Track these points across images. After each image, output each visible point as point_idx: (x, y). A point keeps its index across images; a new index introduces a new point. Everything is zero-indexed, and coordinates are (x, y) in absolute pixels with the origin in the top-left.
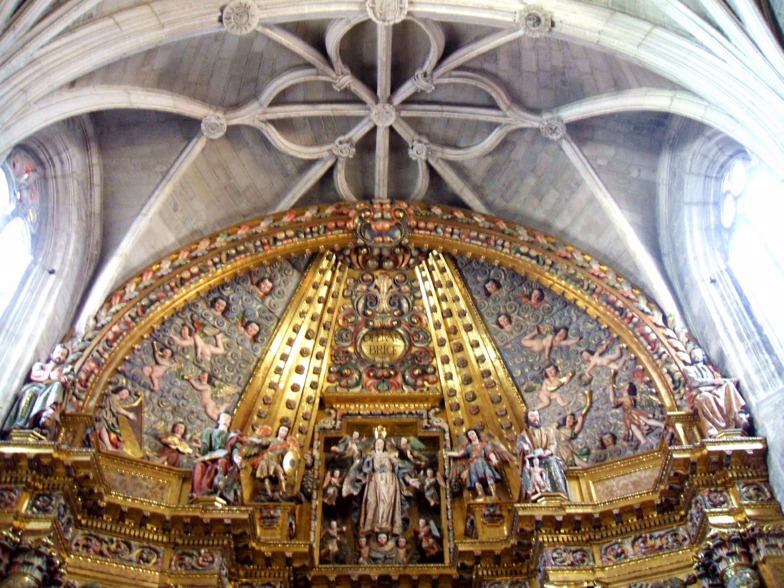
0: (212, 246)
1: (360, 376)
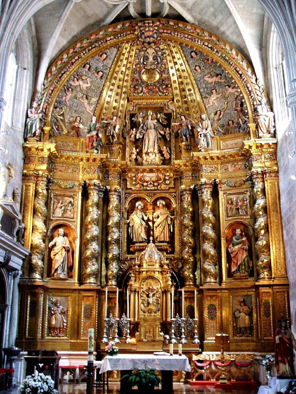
0: (82, 46)
1: (142, 89)
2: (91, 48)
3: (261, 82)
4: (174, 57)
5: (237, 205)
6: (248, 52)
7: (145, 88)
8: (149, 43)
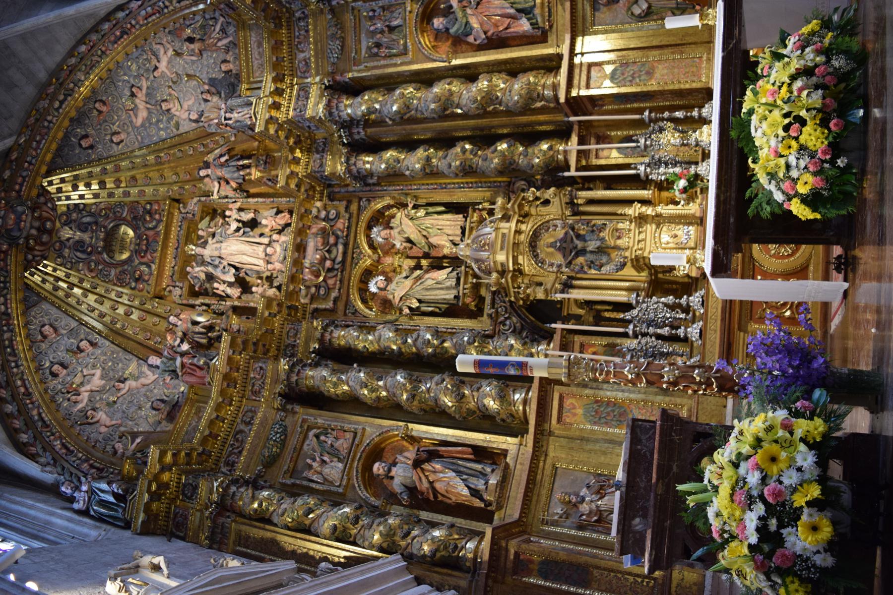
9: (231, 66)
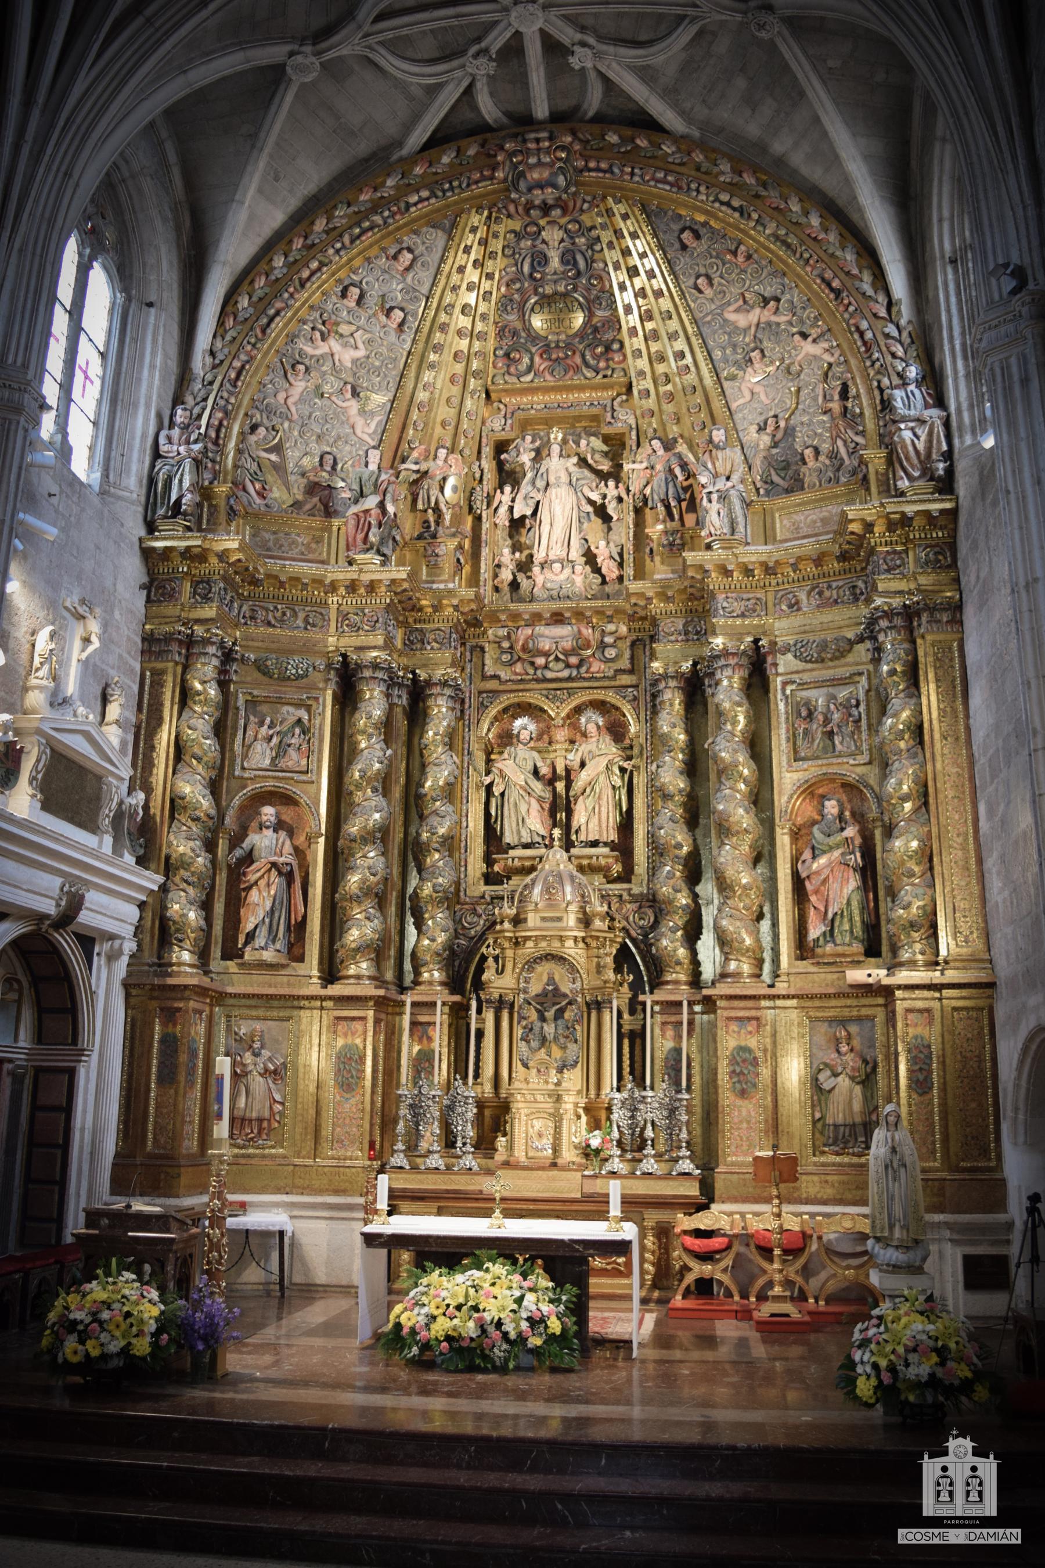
0: (331, 226)
1: (532, 360)
2: (357, 230)
3: (906, 313)
4: (626, 253)
5: (827, 721)
6: (863, 218)
7: (541, 356)
8: (546, 209)
9: (811, 463)
